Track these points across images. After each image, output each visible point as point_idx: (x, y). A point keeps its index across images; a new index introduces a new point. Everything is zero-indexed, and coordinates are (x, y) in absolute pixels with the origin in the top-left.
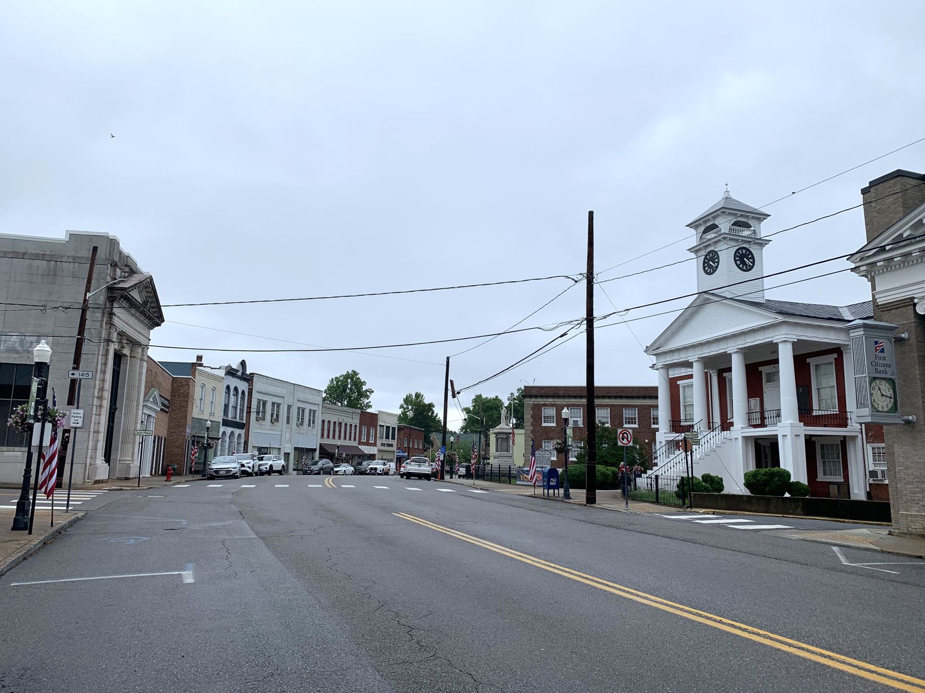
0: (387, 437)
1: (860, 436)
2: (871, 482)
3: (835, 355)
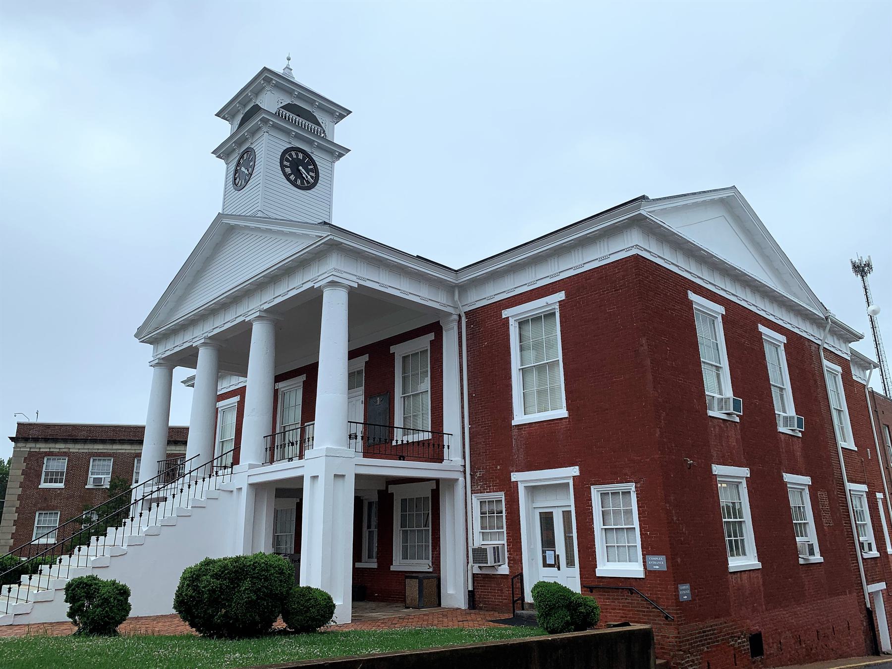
0: (736, 541)
1: (461, 479)
2: (476, 571)
3: (431, 336)
